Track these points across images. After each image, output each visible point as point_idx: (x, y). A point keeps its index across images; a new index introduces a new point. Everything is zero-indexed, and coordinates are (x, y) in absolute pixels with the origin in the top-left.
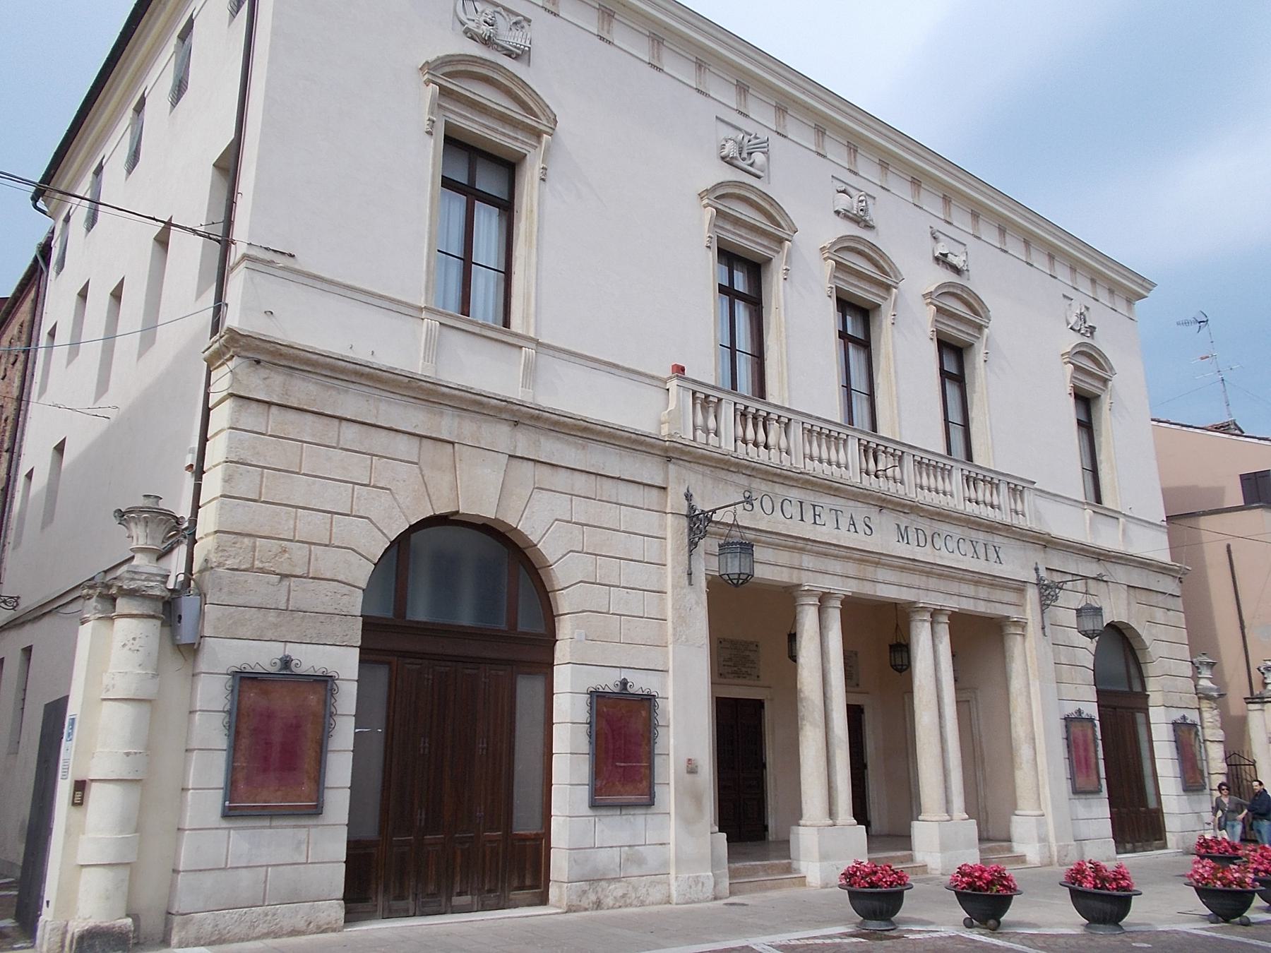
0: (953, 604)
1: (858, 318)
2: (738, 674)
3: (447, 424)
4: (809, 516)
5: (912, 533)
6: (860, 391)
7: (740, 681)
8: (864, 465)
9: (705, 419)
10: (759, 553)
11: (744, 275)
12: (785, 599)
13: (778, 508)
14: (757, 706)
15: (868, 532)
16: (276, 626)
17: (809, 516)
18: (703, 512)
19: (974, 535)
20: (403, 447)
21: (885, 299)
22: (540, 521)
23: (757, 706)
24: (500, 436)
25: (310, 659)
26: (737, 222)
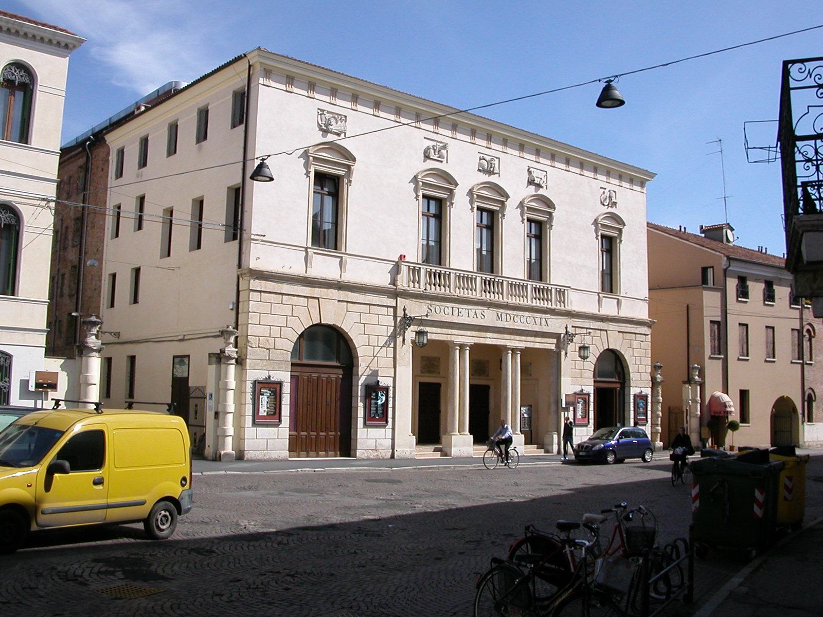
0: (522, 345)
1: (490, 222)
2: (429, 372)
3: (317, 292)
4: (456, 313)
5: (504, 315)
6: (489, 259)
7: (430, 375)
8: (534, 296)
9: (560, 297)
10: (571, 296)
11: (437, 210)
12: (445, 347)
13: (442, 311)
14: (437, 386)
15: (483, 317)
16: (265, 365)
17: (456, 313)
18: (410, 317)
19: (535, 315)
20: (303, 301)
21: (645, 425)
22: (350, 326)
23: (437, 386)
24: (334, 293)
25: (276, 376)
26: (431, 186)
